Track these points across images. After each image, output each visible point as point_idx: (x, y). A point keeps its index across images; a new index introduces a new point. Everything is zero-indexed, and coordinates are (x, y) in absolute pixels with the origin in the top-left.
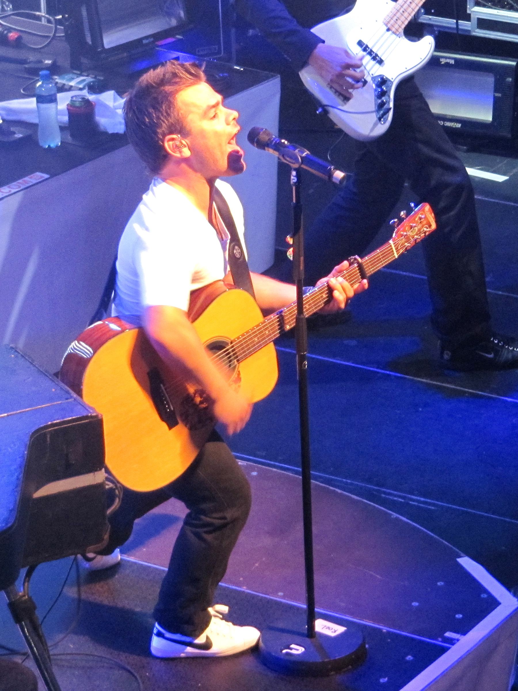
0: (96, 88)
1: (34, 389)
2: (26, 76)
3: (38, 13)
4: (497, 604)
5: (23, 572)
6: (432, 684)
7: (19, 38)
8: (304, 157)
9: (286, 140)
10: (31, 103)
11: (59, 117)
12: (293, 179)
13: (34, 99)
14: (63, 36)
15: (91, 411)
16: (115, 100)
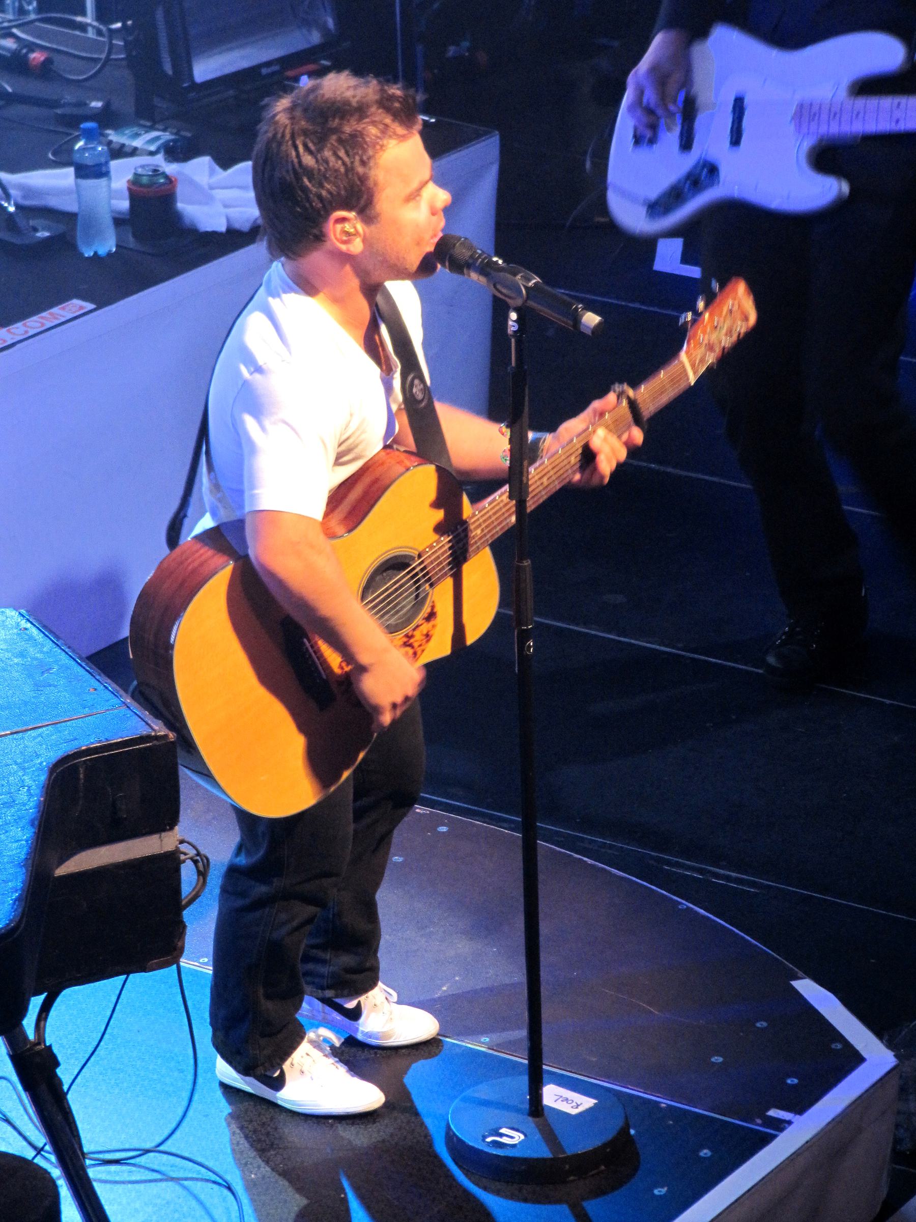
0: (178, 152)
3: (79, 19)
4: (860, 1059)
6: (725, 1214)
7: (48, 62)
8: (531, 288)
9: (500, 258)
10: (64, 177)
11: (113, 202)
13: (71, 170)
14: (122, 59)
16: (212, 173)
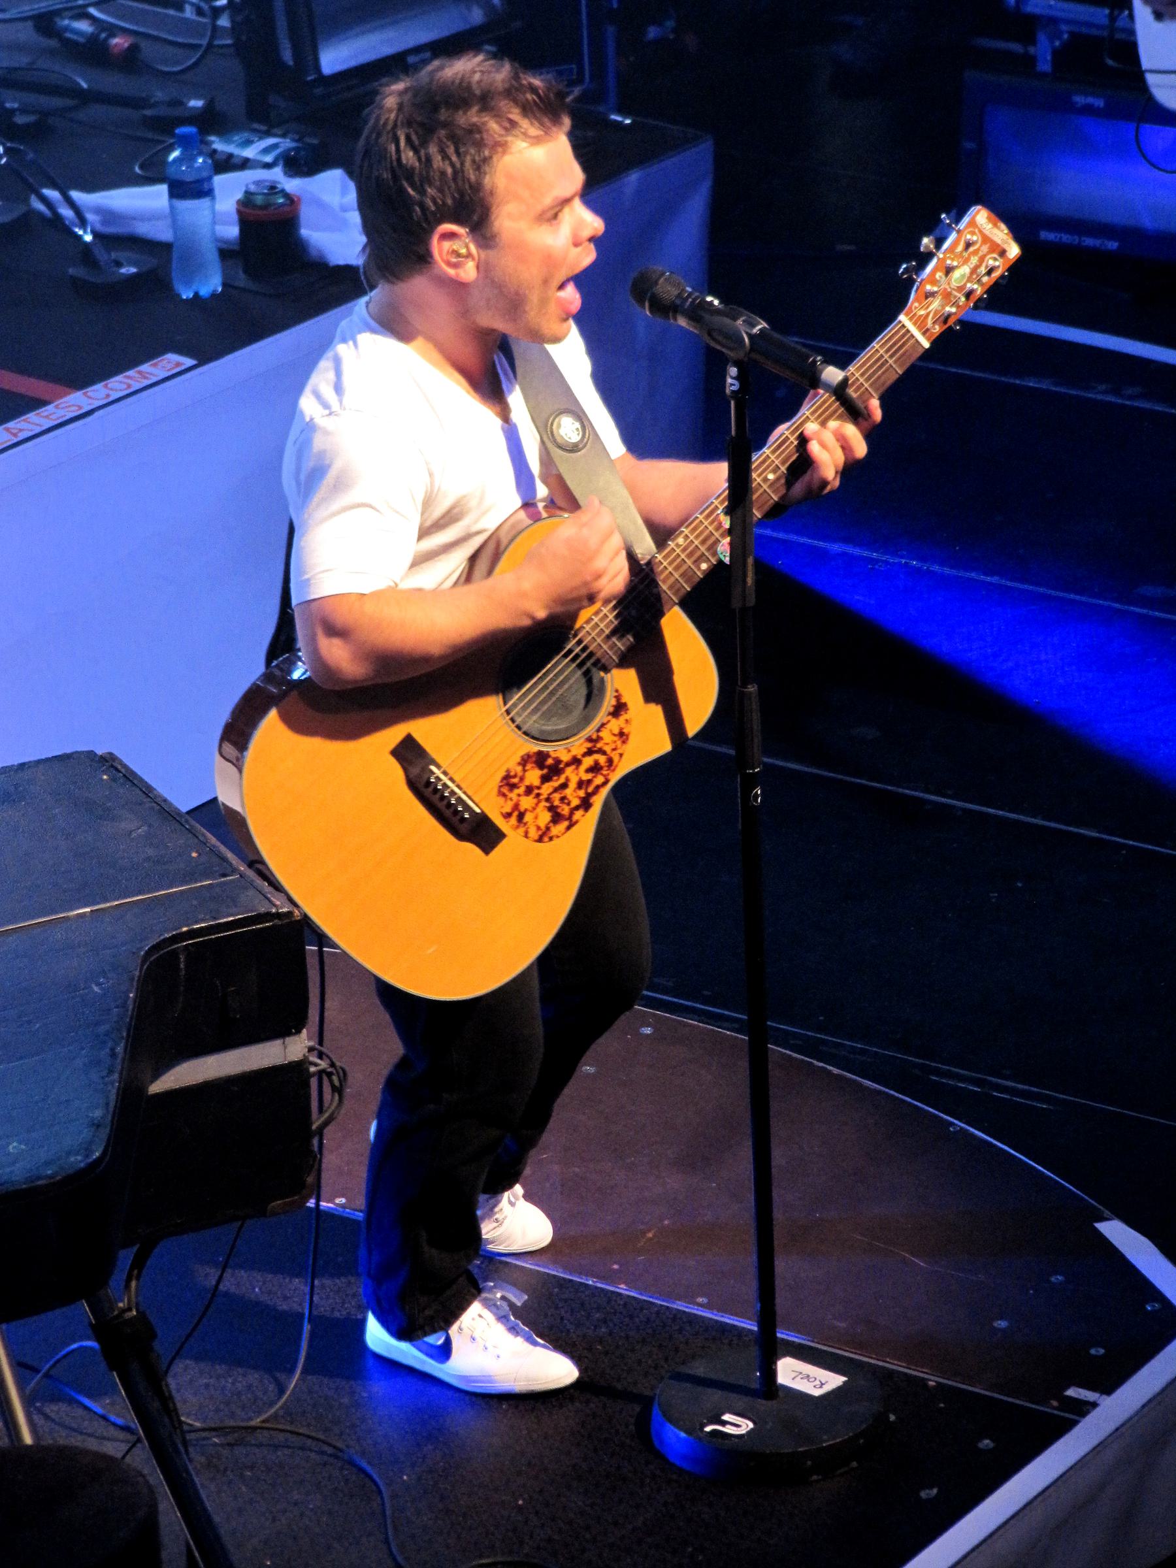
0: (301, 164)
1: (150, 852)
2: (150, 135)
5: (126, 1257)
7: (134, 48)
10: (155, 197)
12: (731, 383)
13: (163, 188)
15: (278, 903)
